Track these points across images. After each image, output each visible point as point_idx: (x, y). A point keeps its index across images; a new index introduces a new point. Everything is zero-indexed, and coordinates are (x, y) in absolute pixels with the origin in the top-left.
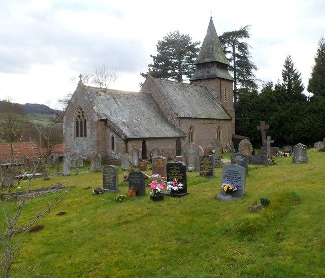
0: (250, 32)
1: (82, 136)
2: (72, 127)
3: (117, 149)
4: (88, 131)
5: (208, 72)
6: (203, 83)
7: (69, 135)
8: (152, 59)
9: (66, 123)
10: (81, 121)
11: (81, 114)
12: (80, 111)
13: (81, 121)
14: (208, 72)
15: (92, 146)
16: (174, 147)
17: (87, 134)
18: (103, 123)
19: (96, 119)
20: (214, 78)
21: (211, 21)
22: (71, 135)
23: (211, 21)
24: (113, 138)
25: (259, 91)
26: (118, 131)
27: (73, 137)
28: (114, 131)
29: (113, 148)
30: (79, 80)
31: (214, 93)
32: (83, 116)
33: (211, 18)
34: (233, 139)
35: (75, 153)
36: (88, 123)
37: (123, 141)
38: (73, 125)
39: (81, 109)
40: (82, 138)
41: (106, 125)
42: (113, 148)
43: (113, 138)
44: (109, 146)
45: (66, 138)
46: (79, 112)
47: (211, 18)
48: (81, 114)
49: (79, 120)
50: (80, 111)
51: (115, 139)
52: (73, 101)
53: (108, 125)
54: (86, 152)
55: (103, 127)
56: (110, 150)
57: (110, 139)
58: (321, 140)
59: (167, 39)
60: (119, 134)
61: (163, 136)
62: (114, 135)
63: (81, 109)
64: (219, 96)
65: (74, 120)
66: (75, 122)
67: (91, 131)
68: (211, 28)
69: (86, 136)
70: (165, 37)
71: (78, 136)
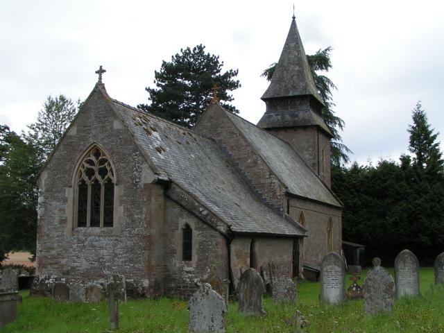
0: (333, 58)
1: (95, 223)
2: (65, 201)
3: (200, 260)
4: (119, 211)
5: (293, 115)
6: (282, 134)
7: (56, 223)
8: (148, 95)
9: (47, 191)
10: (96, 185)
11: (98, 166)
12: (93, 158)
13: (96, 185)
14: (283, 117)
15: (130, 250)
16: (291, 259)
17: (116, 217)
18: (161, 191)
19: (148, 177)
20: (308, 127)
21: (294, 25)
22: (63, 221)
23: (294, 25)
24: (187, 232)
25: (349, 166)
26: (205, 213)
27: (69, 226)
28: (191, 212)
29: (187, 256)
30: (97, 81)
31: (307, 156)
32: (103, 172)
33: (294, 18)
34: (344, 247)
35: (73, 268)
36: (117, 190)
37: (220, 240)
38: (71, 194)
39: (97, 154)
40: (96, 230)
41: (167, 197)
42: (187, 256)
43: (187, 232)
44: (174, 252)
45: (45, 230)
46: (91, 162)
47: (294, 18)
48: (98, 166)
49: (89, 183)
50: (93, 158)
51: (195, 233)
52: (73, 132)
53: (174, 197)
54: (109, 268)
55: (161, 199)
56: (177, 262)
57: (179, 233)
58: (426, 259)
59: (178, 61)
60: (208, 221)
61: (278, 232)
62: (193, 223)
63: (97, 154)
64: (316, 161)
65: (75, 181)
66: (77, 188)
67: (127, 210)
68: (293, 38)
69: (109, 223)
70: (177, 56)
71: (82, 223)
